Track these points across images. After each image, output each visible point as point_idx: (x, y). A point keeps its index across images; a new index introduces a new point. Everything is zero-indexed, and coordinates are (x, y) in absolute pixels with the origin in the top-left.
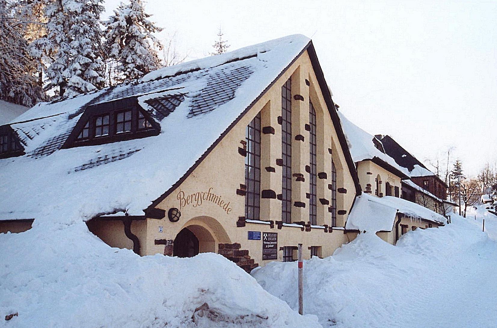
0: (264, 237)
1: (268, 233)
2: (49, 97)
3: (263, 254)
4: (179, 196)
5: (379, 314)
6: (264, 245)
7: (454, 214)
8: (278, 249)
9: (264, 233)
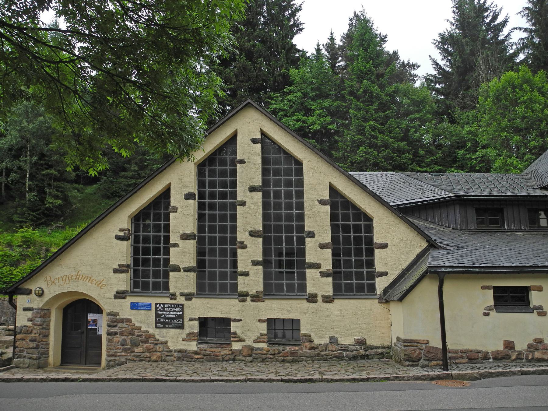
0: (157, 308)
1: (164, 304)
3: (156, 323)
4: (46, 279)
6: (158, 316)
7: (247, 204)
9: (156, 304)
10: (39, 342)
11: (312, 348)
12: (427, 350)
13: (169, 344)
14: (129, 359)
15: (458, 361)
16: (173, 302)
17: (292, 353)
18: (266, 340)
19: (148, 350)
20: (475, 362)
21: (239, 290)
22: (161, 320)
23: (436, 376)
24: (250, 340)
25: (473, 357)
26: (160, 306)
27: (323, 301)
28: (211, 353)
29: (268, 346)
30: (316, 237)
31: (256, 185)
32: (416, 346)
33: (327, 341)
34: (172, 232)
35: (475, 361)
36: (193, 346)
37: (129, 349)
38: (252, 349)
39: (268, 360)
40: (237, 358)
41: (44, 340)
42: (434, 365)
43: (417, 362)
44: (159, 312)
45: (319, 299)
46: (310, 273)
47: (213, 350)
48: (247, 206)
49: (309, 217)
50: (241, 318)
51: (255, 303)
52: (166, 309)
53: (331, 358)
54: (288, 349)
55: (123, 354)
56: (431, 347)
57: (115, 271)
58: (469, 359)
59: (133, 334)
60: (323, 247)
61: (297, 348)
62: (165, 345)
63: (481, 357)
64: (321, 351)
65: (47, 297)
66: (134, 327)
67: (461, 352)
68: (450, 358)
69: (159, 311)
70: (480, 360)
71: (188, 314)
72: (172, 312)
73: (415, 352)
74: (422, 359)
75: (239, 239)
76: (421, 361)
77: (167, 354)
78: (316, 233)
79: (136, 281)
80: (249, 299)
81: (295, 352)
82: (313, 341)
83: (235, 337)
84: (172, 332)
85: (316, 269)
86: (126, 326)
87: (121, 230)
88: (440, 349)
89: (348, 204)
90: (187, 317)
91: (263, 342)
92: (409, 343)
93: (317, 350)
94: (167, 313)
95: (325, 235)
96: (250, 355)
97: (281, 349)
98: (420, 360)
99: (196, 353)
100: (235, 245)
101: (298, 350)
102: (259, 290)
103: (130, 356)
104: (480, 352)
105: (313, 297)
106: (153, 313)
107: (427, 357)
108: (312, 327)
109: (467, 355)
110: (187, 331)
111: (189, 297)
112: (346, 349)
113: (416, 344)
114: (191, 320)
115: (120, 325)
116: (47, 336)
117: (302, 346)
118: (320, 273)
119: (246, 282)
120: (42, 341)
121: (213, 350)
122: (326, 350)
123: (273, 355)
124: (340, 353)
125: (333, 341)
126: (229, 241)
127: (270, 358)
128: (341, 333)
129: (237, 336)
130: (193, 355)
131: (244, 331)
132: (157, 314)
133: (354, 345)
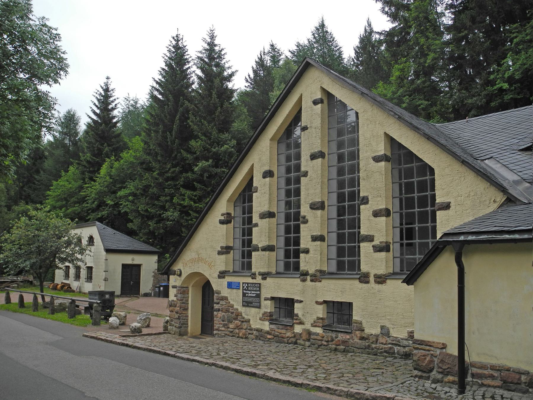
0: (243, 287)
1: (248, 283)
2: (62, 128)
3: (243, 302)
5: (384, 362)
6: (244, 295)
7: (309, 174)
8: (262, 299)
9: (243, 283)
10: (180, 314)
11: (362, 338)
12: (440, 358)
13: (251, 322)
14: (226, 334)
15: (486, 382)
16: (254, 281)
17: (344, 342)
18: (321, 325)
19: (237, 327)
20: (513, 388)
21: (301, 269)
22: (246, 299)
23: (372, 397)
24: (308, 323)
25: (510, 380)
26: (245, 285)
27: (376, 282)
28: (278, 334)
29: (324, 332)
30: (370, 203)
31: (316, 151)
32: (429, 350)
33: (376, 331)
34: (254, 212)
35: (513, 387)
36: (266, 326)
37: (226, 325)
38: (309, 333)
39: (323, 347)
40: (298, 341)
41: (184, 312)
42: (449, 382)
43: (428, 373)
44: (245, 291)
45: (372, 279)
46: (365, 248)
47: (280, 331)
48: (308, 176)
49: (364, 179)
50: (302, 300)
51: (313, 283)
52: (249, 288)
53: (381, 353)
54: (340, 337)
55: (223, 329)
56: (448, 354)
57: (219, 253)
58: (505, 382)
59: (229, 312)
60: (377, 214)
61: (348, 337)
62: (248, 323)
63: (525, 383)
64: (372, 343)
65: (184, 276)
66: (229, 305)
67: (491, 369)
68: (473, 375)
69: (244, 290)
70: (523, 386)
71: (266, 293)
72: (253, 291)
73: (425, 359)
74: (435, 370)
75: (302, 214)
76: (433, 373)
77: (249, 332)
78: (370, 198)
79: (341, 261)
80: (309, 278)
81: (346, 341)
82: (364, 330)
83: (296, 319)
84: (253, 310)
85: (370, 243)
86: (225, 303)
87: (222, 215)
88: (455, 356)
89: (411, 156)
90: (263, 297)
91: (319, 327)
92: (419, 344)
93: (367, 341)
94: (250, 292)
95: (379, 199)
96: (309, 340)
97: (334, 336)
98: (431, 370)
99: (268, 333)
100: (299, 220)
101: (349, 339)
102: (317, 269)
103: (227, 331)
104: (523, 374)
105: (365, 277)
106: (241, 291)
107: (441, 368)
108: (364, 313)
109: (501, 374)
110: (263, 310)
111: (265, 276)
112: (397, 343)
113: (428, 348)
114: (266, 299)
115: (221, 302)
116: (187, 309)
117: (353, 335)
118: (373, 246)
119: (307, 260)
120: (182, 313)
121: (280, 331)
122: (377, 342)
123: (328, 341)
124: (391, 348)
125: (383, 332)
126: (430, 216)
127: (324, 345)
128: (393, 323)
129: (299, 318)
130: (266, 335)
131: (304, 314)
132: (243, 292)
133: (406, 340)
